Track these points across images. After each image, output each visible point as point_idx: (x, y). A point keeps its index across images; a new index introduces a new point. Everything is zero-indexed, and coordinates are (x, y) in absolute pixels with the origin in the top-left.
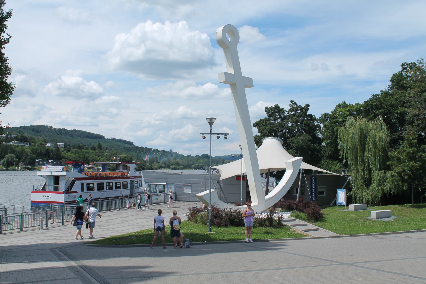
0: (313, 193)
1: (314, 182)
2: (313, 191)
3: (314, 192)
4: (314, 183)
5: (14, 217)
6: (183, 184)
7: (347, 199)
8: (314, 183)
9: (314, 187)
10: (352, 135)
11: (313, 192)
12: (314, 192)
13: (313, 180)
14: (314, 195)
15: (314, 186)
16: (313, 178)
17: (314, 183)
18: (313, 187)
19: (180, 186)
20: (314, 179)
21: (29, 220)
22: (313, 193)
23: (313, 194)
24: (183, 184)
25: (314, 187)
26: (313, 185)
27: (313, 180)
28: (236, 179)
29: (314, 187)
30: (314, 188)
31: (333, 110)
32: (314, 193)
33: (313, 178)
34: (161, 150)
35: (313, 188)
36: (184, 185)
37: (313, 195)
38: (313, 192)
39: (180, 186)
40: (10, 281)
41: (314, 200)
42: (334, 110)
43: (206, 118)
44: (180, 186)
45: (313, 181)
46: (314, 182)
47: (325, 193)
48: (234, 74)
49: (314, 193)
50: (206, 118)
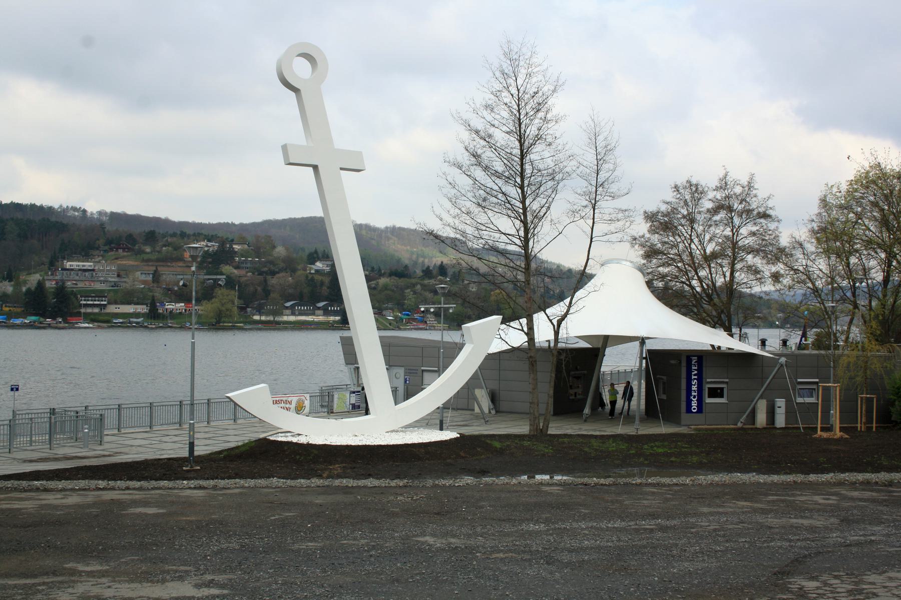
0: (695, 375)
1: (693, 399)
2: (695, 379)
4: (692, 398)
6: (422, 368)
7: (704, 391)
9: (694, 388)
10: (420, 506)
11: (696, 377)
12: (693, 377)
13: (694, 404)
14: (693, 368)
15: (694, 391)
16: (694, 409)
17: (694, 397)
22: (695, 375)
23: (696, 372)
24: (422, 368)
25: (694, 388)
26: (696, 394)
27: (694, 404)
29: (693, 389)
30: (694, 385)
33: (694, 409)
34: (33, 203)
35: (696, 386)
36: (423, 371)
37: (696, 368)
38: (696, 377)
39: (416, 373)
40: (260, 316)
43: (396, 405)
44: (416, 373)
49: (693, 373)
50: (396, 405)
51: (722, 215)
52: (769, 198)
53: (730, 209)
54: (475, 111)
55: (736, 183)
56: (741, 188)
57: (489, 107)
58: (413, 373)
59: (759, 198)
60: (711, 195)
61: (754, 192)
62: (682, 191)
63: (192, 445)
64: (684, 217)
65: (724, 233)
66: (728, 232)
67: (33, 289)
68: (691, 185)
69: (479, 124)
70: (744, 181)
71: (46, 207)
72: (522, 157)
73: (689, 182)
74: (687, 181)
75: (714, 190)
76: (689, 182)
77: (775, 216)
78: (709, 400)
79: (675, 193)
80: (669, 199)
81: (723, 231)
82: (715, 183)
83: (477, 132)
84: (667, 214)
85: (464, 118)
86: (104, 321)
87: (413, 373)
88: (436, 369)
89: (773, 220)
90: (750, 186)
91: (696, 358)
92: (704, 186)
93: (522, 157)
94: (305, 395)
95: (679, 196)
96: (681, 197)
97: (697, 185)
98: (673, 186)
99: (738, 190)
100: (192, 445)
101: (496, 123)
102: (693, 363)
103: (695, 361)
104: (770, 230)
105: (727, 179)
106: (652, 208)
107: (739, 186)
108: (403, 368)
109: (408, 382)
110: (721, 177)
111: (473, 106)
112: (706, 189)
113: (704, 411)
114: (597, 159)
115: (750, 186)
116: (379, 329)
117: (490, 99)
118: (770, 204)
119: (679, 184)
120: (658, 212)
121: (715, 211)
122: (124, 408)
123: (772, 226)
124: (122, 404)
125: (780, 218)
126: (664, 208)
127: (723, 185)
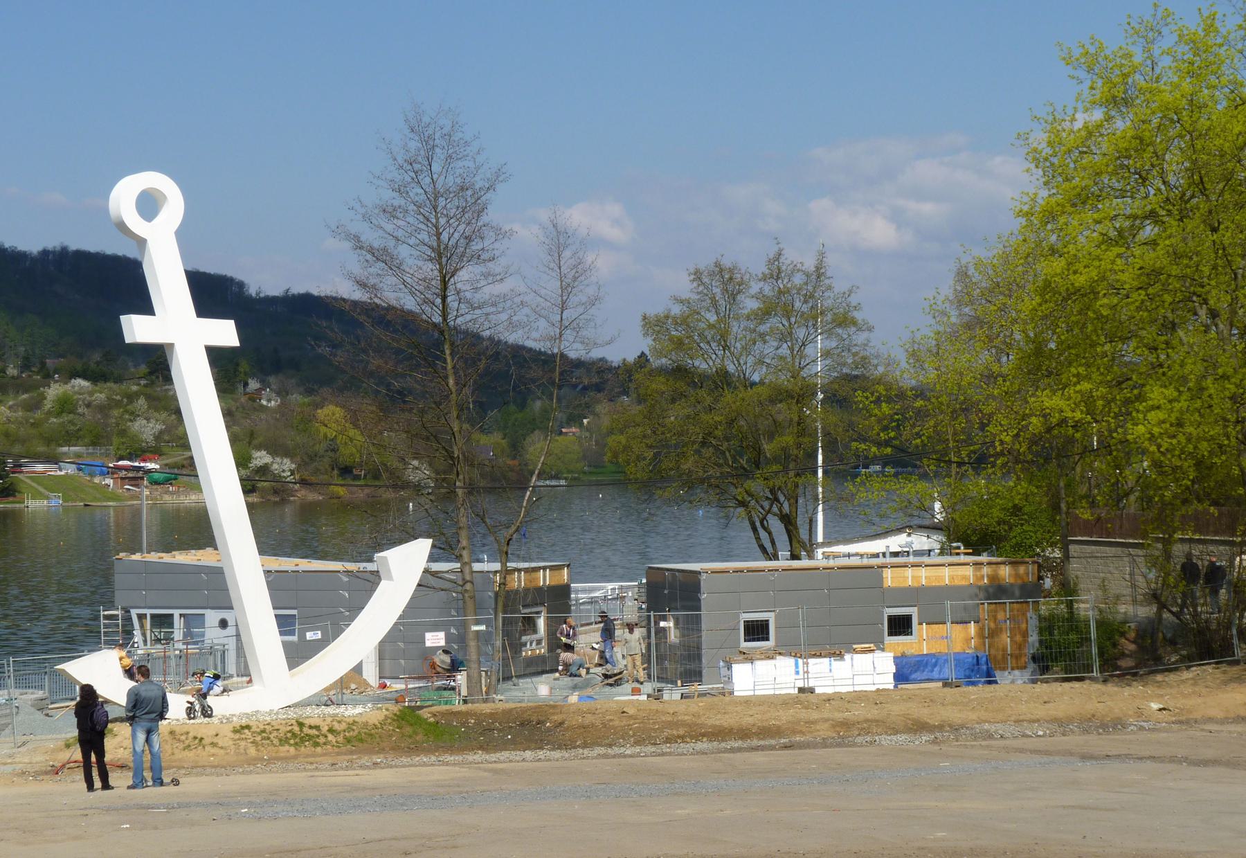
51: (775, 322)
52: (851, 292)
53: (788, 312)
54: (366, 218)
55: (795, 270)
56: (804, 277)
57: (390, 212)
59: (836, 291)
60: (755, 287)
61: (827, 282)
62: (706, 280)
63: (852, 659)
64: (711, 326)
65: (780, 351)
66: (784, 350)
68: (721, 271)
69: (372, 237)
70: (810, 264)
72: (445, 283)
73: (717, 264)
74: (716, 263)
75: (760, 280)
76: (717, 264)
77: (863, 320)
79: (695, 284)
80: (685, 295)
81: (777, 349)
82: (761, 268)
83: (371, 251)
84: (683, 321)
85: (353, 232)
86: (238, 689)
89: (859, 329)
90: (819, 272)
92: (743, 271)
93: (445, 283)
95: (701, 288)
96: (705, 291)
97: (731, 271)
98: (692, 270)
99: (798, 280)
100: (852, 659)
101: (400, 233)
104: (856, 345)
105: (781, 261)
106: (656, 309)
107: (800, 273)
110: (771, 256)
112: (746, 277)
114: (562, 288)
115: (819, 272)
116: (282, 633)
117: (389, 196)
118: (854, 300)
119: (702, 267)
120: (667, 317)
121: (765, 313)
123: (860, 338)
125: (871, 324)
126: (676, 310)
127: (775, 274)
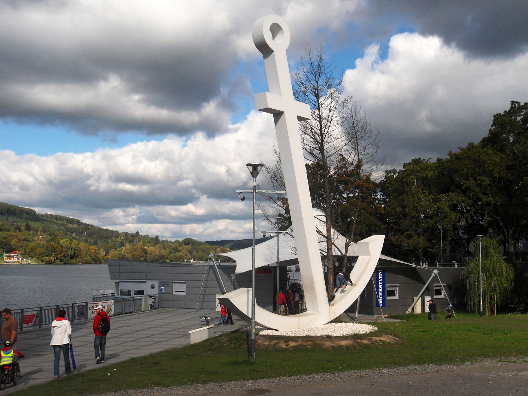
0: (381, 282)
1: (380, 298)
2: (381, 284)
3: (380, 283)
4: (379, 297)
5: (15, 315)
8: (381, 296)
11: (381, 283)
12: (380, 283)
14: (380, 277)
15: (381, 292)
17: (381, 296)
18: (382, 291)
19: (169, 283)
20: (380, 303)
21: (471, 305)
22: (381, 282)
23: (381, 280)
24: (173, 281)
25: (381, 290)
26: (382, 294)
28: (258, 273)
29: (380, 291)
30: (381, 288)
31: (490, 128)
32: (380, 281)
33: (381, 304)
35: (382, 289)
36: (173, 283)
37: (381, 277)
38: (381, 283)
39: (169, 285)
41: (380, 271)
42: (492, 126)
44: (169, 285)
45: (382, 299)
46: (379, 298)
47: (397, 293)
48: (383, 237)
49: (380, 281)
58: (166, 284)
67: (145, 141)
71: (453, 45)
78: (388, 298)
87: (166, 284)
88: (185, 281)
91: (381, 271)
94: (111, 301)
102: (380, 274)
103: (380, 273)
108: (158, 281)
109: (163, 291)
111: (301, 82)
113: (386, 306)
122: (13, 313)
124: (59, 305)
